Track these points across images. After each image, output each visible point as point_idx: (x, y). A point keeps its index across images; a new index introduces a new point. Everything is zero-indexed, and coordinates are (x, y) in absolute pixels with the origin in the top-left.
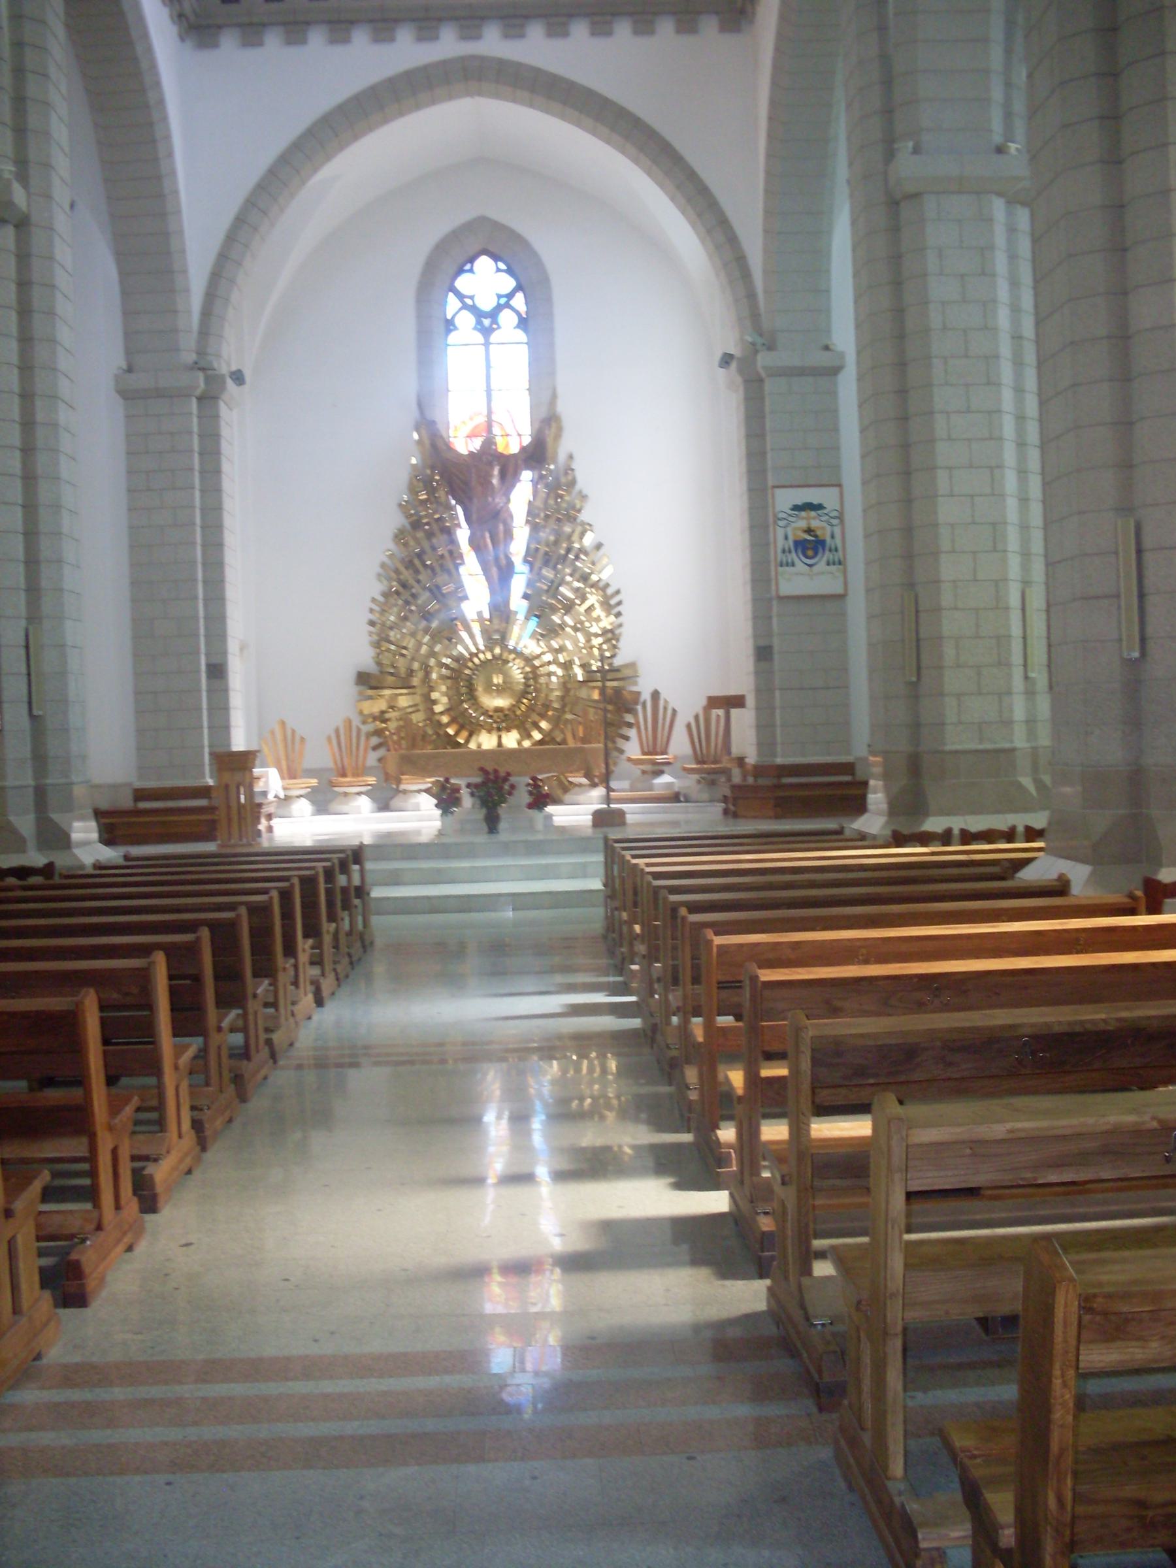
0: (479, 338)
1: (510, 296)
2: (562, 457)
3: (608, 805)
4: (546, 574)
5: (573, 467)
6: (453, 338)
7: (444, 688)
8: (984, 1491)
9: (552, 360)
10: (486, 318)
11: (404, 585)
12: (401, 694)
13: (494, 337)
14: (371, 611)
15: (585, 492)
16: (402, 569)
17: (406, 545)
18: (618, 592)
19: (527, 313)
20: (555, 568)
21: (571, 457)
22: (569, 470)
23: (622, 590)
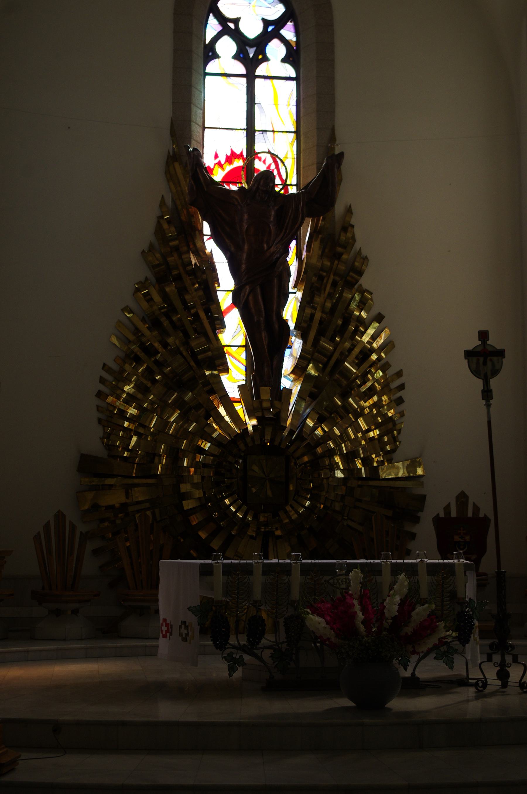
0: (240, 68)
1: (280, 23)
2: (339, 208)
3: (136, 463)
4: (194, 554)
5: (352, 222)
6: (212, 67)
7: (197, 479)
8: (135, 391)
9: (331, 79)
10: (251, 46)
11: (150, 351)
12: (138, 485)
13: (261, 70)
14: (102, 381)
15: (364, 253)
16: (144, 328)
17: (148, 298)
18: (399, 374)
19: (297, 42)
20: (332, 340)
21: (349, 211)
22: (347, 227)
23: (404, 373)
